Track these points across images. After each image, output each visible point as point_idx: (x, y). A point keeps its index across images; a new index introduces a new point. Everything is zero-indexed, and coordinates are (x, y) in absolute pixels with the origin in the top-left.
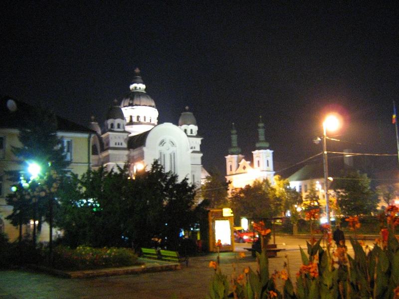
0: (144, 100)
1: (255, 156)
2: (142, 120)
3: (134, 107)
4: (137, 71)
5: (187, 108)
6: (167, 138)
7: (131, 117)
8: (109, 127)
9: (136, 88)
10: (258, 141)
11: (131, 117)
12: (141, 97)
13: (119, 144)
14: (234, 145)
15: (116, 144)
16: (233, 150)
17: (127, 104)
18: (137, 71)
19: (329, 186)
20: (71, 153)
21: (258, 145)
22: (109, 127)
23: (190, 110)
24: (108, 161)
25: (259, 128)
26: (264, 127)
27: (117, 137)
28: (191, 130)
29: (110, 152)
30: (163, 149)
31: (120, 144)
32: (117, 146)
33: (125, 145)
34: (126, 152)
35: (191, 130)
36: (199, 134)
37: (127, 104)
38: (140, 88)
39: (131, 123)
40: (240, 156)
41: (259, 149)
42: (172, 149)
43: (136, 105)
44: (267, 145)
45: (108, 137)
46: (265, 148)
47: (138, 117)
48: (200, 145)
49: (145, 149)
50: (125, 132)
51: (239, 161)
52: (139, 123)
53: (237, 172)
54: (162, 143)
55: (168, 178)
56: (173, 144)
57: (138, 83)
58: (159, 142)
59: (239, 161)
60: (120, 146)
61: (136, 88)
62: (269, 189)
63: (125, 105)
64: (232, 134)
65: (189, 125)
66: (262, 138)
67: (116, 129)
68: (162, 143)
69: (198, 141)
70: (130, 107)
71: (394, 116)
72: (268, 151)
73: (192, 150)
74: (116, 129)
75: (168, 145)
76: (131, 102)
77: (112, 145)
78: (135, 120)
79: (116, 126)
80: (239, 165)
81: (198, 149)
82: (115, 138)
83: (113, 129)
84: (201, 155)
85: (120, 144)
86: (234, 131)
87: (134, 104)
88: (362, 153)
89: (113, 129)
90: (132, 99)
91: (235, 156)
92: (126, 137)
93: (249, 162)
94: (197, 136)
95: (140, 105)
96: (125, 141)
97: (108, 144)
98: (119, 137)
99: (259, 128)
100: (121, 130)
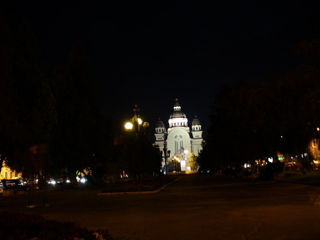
0: (178, 115)
1: (183, 170)
2: (177, 125)
3: (173, 119)
4: (177, 100)
5: (177, 108)
6: (179, 134)
8: (193, 129)
12: (176, 113)
18: (177, 100)
22: (193, 129)
23: (197, 118)
30: (176, 140)
32: (160, 140)
36: (202, 129)
38: (177, 109)
42: (181, 139)
43: (174, 118)
47: (175, 123)
48: (202, 135)
54: (176, 137)
56: (181, 137)
57: (176, 107)
58: (175, 136)
60: (161, 140)
68: (176, 137)
71: (30, 207)
74: (159, 132)
75: (179, 138)
78: (174, 125)
79: (158, 131)
82: (158, 136)
88: (162, 123)
94: (200, 130)
98: (160, 136)
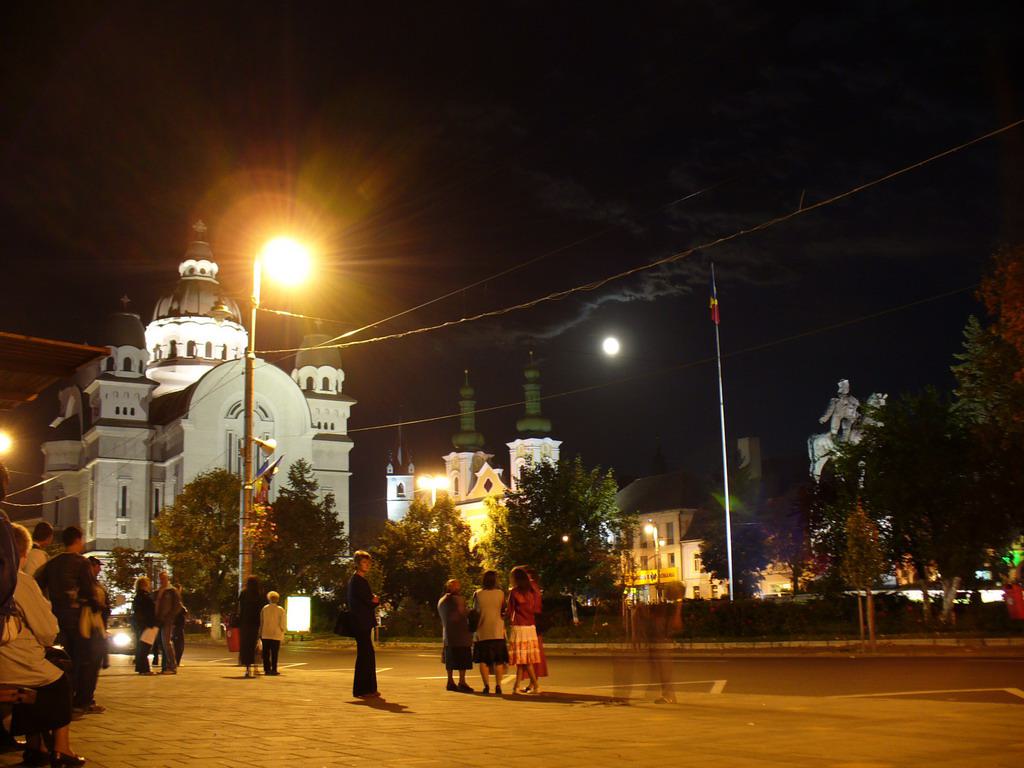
2: (200, 352)
3: (182, 319)
7: (173, 343)
9: (192, 270)
10: (522, 414)
11: (173, 343)
13: (326, 427)
14: (466, 427)
15: (117, 412)
16: (461, 440)
17: (164, 311)
19: (684, 532)
20: (162, 673)
21: (521, 427)
24: (95, 455)
25: (526, 381)
26: (536, 381)
27: (121, 393)
28: (326, 381)
29: (99, 431)
31: (329, 426)
32: (121, 416)
33: (142, 415)
34: (145, 434)
35: (326, 381)
37: (164, 311)
38: (203, 271)
39: (173, 360)
40: (481, 454)
41: (525, 435)
44: (547, 427)
45: (97, 393)
46: (540, 435)
48: (348, 420)
49: (185, 424)
50: (143, 380)
51: (476, 468)
52: (192, 360)
53: (472, 496)
55: (338, 537)
59: (476, 468)
60: (128, 417)
61: (192, 270)
62: (452, 528)
63: (160, 315)
64: (462, 399)
65: (318, 367)
66: (532, 407)
67: (119, 372)
69: (344, 409)
70: (172, 319)
72: (548, 440)
73: (316, 431)
76: (175, 307)
77: (107, 412)
78: (182, 352)
79: (119, 363)
80: (475, 479)
81: (341, 429)
83: (111, 373)
84: (351, 445)
85: (329, 426)
86: (467, 392)
87: (183, 312)
89: (111, 373)
90: (178, 299)
91: (468, 456)
92: (144, 394)
93: (500, 471)
95: (197, 315)
96: (141, 404)
97: (98, 409)
99: (526, 381)
100: (136, 374)
